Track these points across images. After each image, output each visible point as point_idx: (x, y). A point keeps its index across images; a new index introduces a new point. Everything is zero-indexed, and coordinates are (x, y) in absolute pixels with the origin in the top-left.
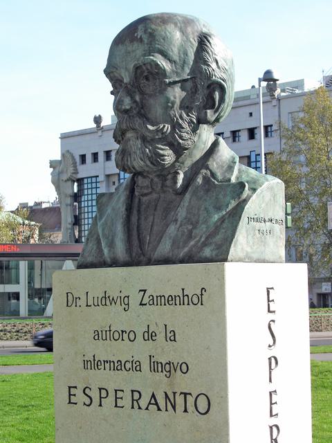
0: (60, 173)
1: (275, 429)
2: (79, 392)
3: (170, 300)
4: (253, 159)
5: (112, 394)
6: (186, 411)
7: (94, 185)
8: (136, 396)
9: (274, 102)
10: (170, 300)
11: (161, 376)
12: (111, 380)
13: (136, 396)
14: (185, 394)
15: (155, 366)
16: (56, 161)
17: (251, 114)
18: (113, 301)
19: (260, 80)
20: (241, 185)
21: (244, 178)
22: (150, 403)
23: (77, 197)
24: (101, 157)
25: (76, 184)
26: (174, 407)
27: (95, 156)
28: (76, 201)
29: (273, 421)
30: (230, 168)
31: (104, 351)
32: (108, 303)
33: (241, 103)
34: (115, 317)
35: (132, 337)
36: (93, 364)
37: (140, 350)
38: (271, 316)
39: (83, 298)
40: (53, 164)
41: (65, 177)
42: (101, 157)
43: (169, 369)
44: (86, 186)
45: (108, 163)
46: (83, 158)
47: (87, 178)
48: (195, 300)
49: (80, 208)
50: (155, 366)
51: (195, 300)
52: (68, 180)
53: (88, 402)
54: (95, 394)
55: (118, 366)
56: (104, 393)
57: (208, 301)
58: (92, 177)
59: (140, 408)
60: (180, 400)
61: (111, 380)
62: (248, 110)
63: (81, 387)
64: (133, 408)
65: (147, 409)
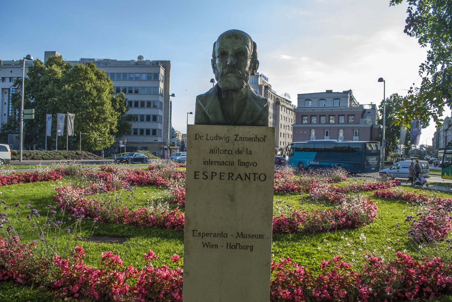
6: (255, 180)
8: (231, 175)
11: (243, 167)
12: (218, 169)
13: (231, 175)
14: (255, 174)
15: (241, 163)
17: (11, 72)
19: (24, 58)
22: (237, 177)
26: (249, 179)
31: (215, 157)
32: (218, 139)
36: (210, 163)
37: (236, 158)
43: (247, 164)
48: (262, 140)
50: (241, 163)
54: (209, 175)
59: (232, 179)
60: (252, 177)
61: (218, 169)
62: (11, 69)
64: (229, 179)
65: (236, 180)
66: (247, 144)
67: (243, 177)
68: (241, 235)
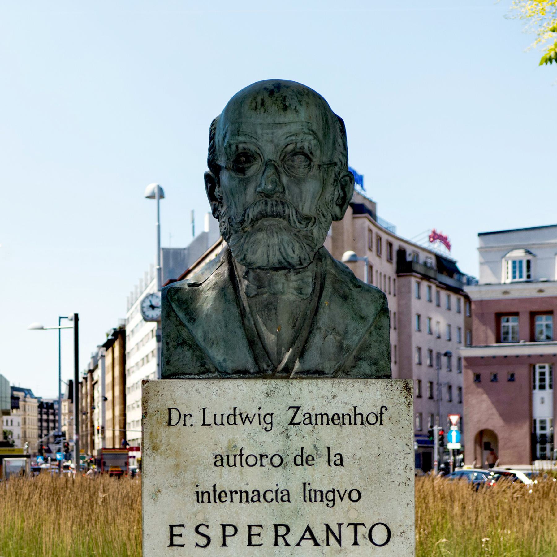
3: (336, 419)
8: (282, 531)
10: (336, 419)
13: (282, 531)
14: (356, 525)
15: (310, 495)
17: (192, 425)
18: (246, 419)
31: (228, 479)
34: (225, 437)
43: (330, 497)
48: (372, 419)
50: (310, 495)
51: (372, 419)
55: (247, 497)
56: (230, 531)
60: (347, 534)
61: (243, 514)
66: (328, 435)
67: (320, 534)
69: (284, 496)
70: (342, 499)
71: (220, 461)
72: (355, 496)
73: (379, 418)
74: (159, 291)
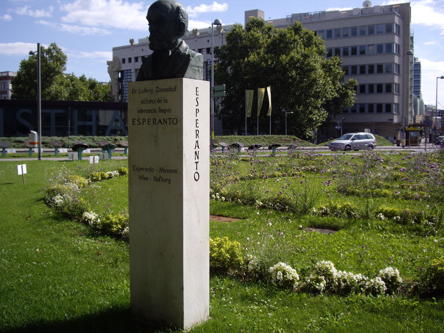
0: (113, 67)
1: (197, 131)
2: (136, 121)
3: (166, 90)
4: (209, 63)
5: (147, 120)
7: (129, 74)
8: (155, 120)
9: (220, 36)
10: (166, 90)
13: (155, 120)
14: (170, 119)
16: (111, 62)
18: (148, 91)
19: (213, 24)
20: (189, 55)
21: (190, 53)
23: (120, 80)
24: (133, 60)
25: (120, 74)
26: (166, 123)
27: (130, 60)
28: (120, 82)
29: (197, 129)
30: (186, 50)
31: (145, 107)
33: (203, 35)
35: (153, 102)
36: (141, 111)
38: (197, 96)
39: (138, 90)
40: (109, 63)
41: (115, 69)
42: (133, 60)
44: (125, 75)
45: (137, 63)
46: (124, 60)
47: (126, 70)
48: (174, 90)
49: (122, 85)
51: (174, 90)
52: (116, 71)
53: (139, 123)
55: (149, 111)
56: (144, 120)
57: (178, 91)
58: (128, 70)
60: (168, 121)
61: (146, 116)
63: (137, 119)
68: (162, 170)
69: (155, 111)
70: (160, 120)
71: (142, 102)
72: (170, 111)
73: (175, 89)
74: (222, 4)
